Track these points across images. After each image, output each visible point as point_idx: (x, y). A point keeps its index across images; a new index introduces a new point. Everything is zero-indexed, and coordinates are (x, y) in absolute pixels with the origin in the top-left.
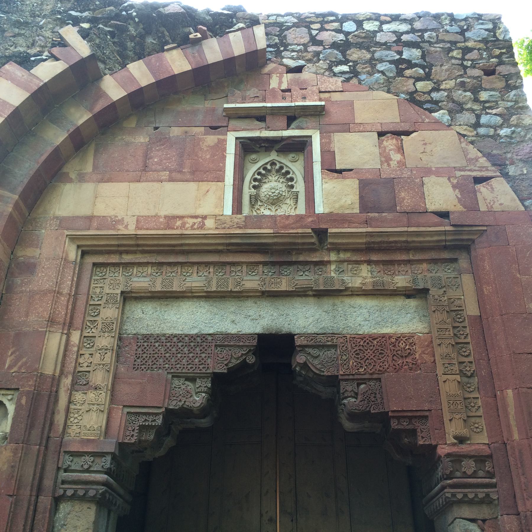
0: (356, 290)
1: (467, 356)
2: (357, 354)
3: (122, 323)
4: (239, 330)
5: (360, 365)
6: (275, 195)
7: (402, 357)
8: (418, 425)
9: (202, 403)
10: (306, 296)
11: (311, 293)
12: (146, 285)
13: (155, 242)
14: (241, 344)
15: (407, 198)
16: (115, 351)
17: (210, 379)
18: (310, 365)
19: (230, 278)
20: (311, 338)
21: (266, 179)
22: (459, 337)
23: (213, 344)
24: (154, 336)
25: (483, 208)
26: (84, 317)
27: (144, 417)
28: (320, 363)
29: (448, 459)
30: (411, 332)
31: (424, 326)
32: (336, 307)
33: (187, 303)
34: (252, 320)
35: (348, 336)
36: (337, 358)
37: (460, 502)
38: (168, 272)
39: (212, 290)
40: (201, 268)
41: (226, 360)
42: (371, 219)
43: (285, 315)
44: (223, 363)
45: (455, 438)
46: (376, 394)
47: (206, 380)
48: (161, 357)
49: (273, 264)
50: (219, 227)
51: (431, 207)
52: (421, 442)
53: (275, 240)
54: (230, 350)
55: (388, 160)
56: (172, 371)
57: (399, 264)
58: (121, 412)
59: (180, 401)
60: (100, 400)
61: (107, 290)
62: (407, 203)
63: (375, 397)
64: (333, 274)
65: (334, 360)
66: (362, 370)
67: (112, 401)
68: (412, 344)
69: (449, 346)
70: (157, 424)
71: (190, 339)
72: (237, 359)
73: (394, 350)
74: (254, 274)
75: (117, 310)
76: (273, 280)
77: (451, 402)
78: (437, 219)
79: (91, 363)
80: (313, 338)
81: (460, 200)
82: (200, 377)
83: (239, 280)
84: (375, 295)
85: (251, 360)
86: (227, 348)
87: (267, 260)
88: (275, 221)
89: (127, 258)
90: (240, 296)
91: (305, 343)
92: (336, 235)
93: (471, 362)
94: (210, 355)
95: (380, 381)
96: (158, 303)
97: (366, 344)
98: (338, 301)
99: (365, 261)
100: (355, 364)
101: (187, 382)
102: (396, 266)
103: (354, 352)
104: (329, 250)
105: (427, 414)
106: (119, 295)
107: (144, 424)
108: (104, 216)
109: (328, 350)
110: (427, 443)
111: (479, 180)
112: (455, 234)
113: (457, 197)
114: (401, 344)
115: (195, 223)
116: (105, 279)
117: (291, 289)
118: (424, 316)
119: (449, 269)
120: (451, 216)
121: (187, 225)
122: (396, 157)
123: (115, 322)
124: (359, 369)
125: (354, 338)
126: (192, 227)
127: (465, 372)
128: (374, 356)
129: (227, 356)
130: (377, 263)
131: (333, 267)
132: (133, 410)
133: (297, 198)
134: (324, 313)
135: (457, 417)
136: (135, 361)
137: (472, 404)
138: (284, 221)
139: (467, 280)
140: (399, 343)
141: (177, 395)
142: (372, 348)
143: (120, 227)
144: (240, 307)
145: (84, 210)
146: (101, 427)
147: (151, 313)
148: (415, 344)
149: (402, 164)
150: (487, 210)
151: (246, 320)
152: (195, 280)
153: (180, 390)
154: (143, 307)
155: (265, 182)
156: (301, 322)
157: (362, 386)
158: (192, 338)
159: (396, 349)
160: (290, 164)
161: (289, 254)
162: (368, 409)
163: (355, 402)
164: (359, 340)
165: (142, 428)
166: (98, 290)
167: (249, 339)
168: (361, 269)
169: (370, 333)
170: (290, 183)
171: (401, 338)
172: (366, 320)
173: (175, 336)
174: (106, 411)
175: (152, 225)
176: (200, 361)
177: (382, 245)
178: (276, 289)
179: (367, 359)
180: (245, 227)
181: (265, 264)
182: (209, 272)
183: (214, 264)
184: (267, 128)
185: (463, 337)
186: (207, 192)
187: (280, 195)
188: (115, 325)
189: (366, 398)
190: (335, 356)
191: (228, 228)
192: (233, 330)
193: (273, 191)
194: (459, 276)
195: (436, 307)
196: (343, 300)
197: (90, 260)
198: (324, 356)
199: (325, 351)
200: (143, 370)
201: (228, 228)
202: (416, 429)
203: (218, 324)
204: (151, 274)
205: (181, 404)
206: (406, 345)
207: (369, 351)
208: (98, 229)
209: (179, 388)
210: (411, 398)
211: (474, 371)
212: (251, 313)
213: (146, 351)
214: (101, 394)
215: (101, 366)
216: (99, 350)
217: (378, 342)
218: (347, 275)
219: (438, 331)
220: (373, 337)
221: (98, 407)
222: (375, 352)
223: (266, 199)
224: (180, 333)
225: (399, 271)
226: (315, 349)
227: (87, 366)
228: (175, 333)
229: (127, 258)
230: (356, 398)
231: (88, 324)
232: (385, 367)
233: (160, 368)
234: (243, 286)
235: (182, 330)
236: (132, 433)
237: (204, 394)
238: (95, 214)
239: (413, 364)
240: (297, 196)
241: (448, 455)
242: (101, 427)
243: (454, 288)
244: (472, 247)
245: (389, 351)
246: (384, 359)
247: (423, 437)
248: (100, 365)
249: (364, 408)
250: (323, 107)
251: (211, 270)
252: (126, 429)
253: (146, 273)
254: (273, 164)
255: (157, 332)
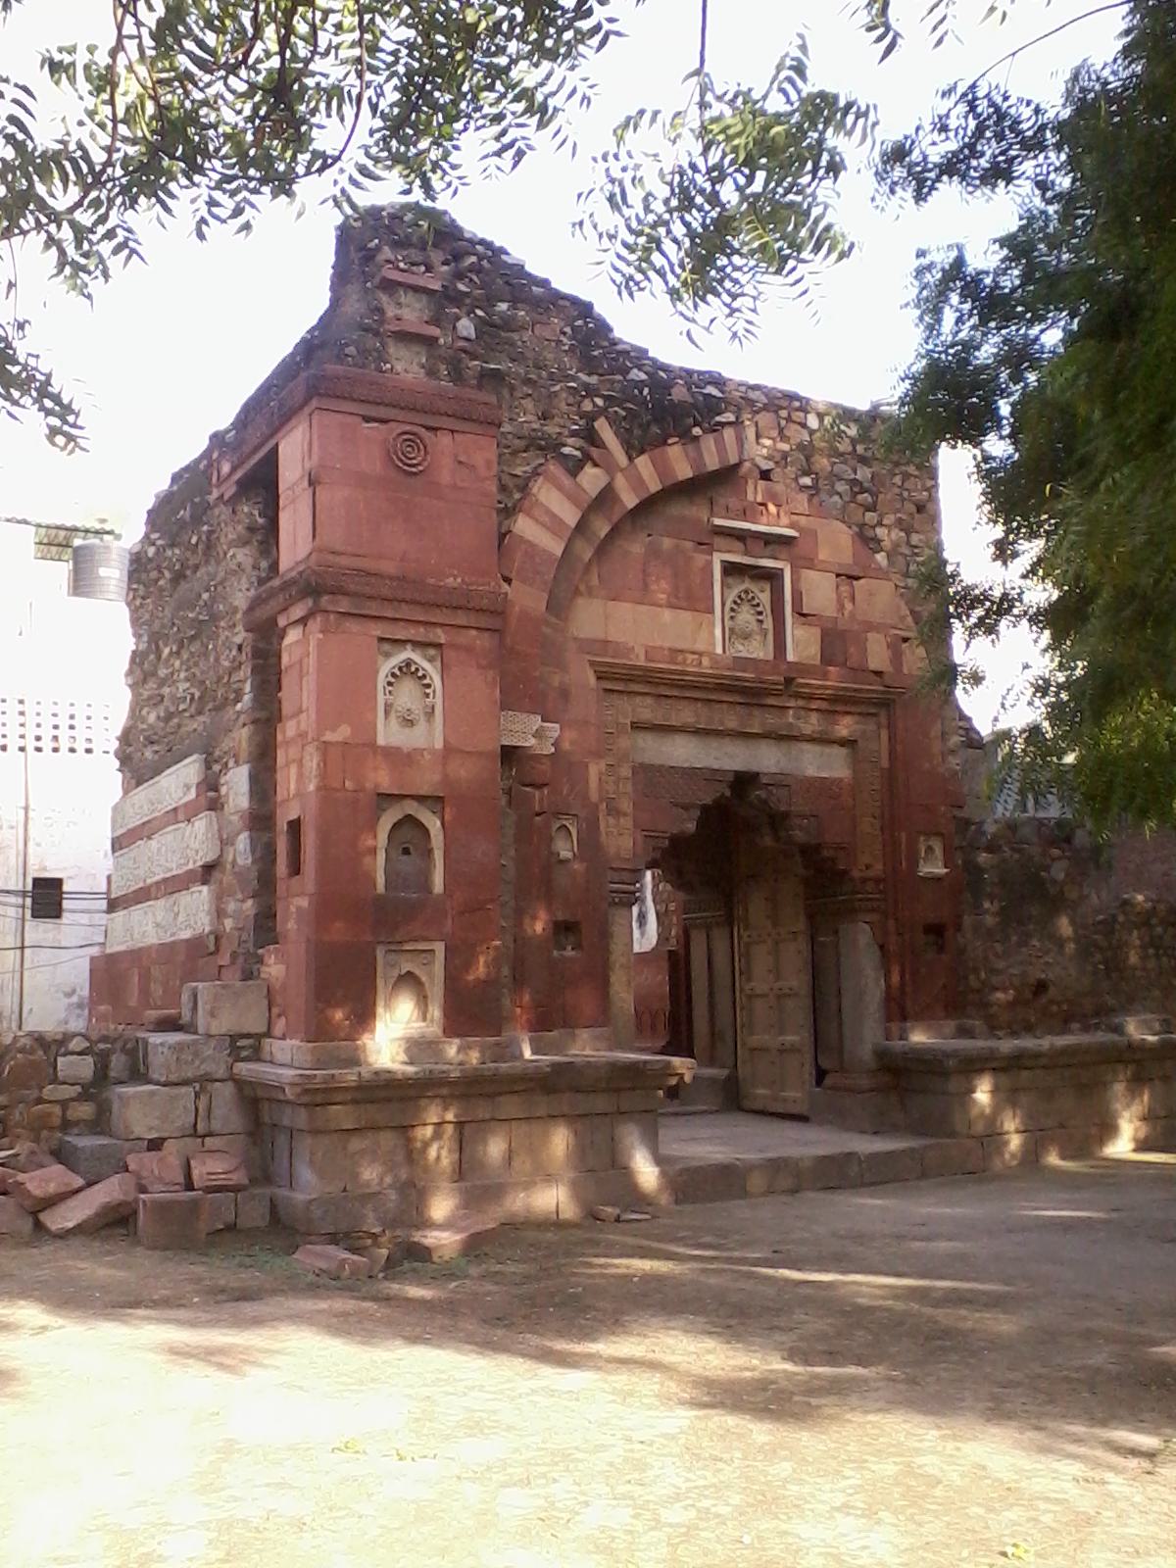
25: (905, 671)
34: (732, 757)
55: (841, 607)
64: (791, 720)
111: (906, 640)
122: (849, 606)
131: (791, 712)
149: (852, 615)
160: (756, 591)
161: (749, 693)
184: (747, 553)
213: (650, 776)
250: (795, 538)
254: (746, 592)
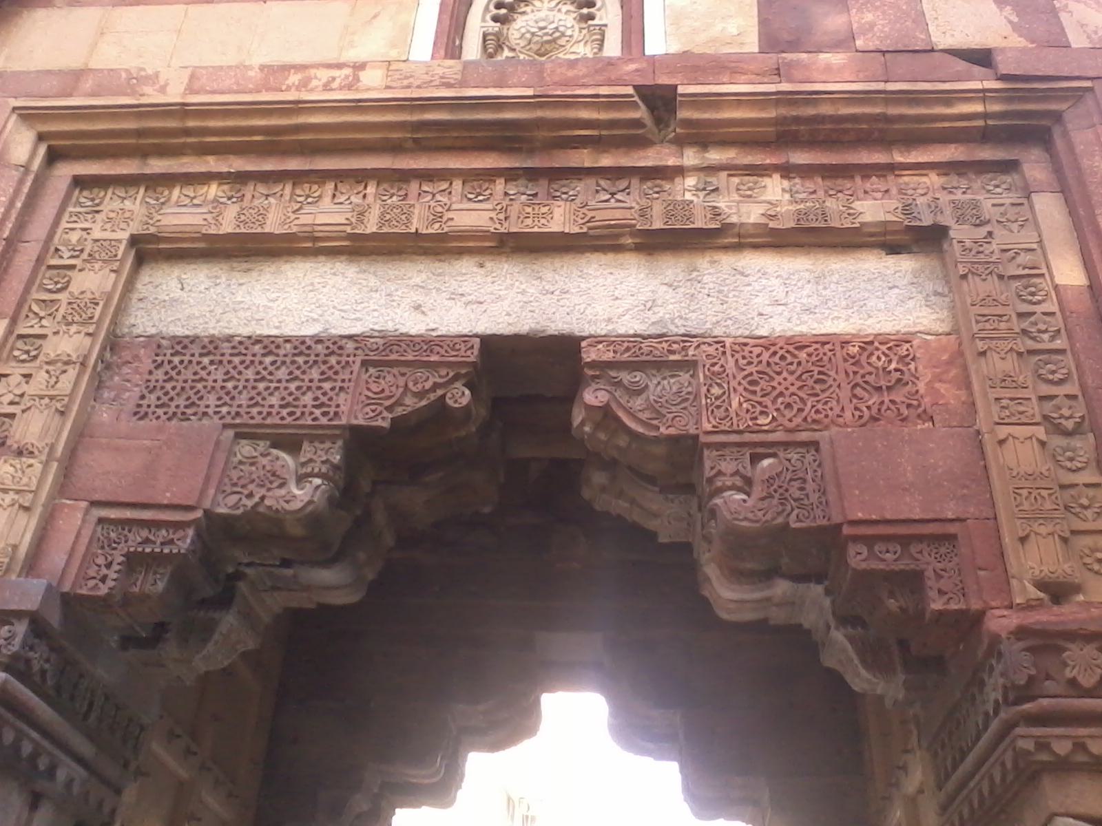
0: (752, 232)
1: (1061, 382)
2: (752, 383)
3: (121, 309)
4: (433, 326)
5: (759, 408)
6: (546, 34)
7: (879, 389)
8: (927, 560)
9: (310, 502)
10: (618, 249)
11: (629, 241)
12: (198, 220)
13: (231, 123)
14: (434, 358)
15: (881, 22)
16: (89, 370)
17: (340, 443)
18: (621, 414)
19: (417, 206)
20: (626, 345)
21: (527, 5)
22: (1034, 339)
23: (358, 360)
24: (202, 341)
25: (1077, 40)
26: (27, 290)
27: (145, 533)
28: (653, 408)
29: (1021, 645)
30: (903, 330)
31: (939, 316)
32: (695, 274)
33: (301, 265)
35: (728, 341)
36: (697, 396)
37: (1063, 767)
38: (257, 194)
39: (368, 231)
40: (343, 187)
41: (390, 397)
42: (790, 65)
43: (557, 293)
44: (380, 404)
45: (1041, 585)
46: (804, 481)
47: (328, 445)
48: (213, 388)
49: (532, 174)
50: (394, 84)
51: (943, 39)
52: (937, 605)
53: (539, 114)
54: (403, 375)
56: (238, 421)
57: (866, 177)
58: (80, 515)
59: (250, 495)
60: (25, 480)
61: (97, 234)
62: (882, 31)
63: (802, 489)
65: (687, 400)
66: (763, 420)
67: (64, 486)
68: (908, 360)
69: (1009, 355)
70: (175, 551)
71: (295, 348)
72: (421, 395)
73: (855, 373)
74: (481, 198)
75: (113, 275)
76: (529, 210)
77: (1024, 492)
78: (961, 65)
79: (22, 395)
80: (631, 345)
81: (1016, 28)
82: (312, 439)
83: (439, 209)
84: (802, 246)
85: (460, 397)
86: (395, 371)
87: (517, 165)
88: (541, 72)
89: (157, 166)
90: (439, 247)
91: (608, 356)
92: (697, 101)
93: (1074, 397)
94: (345, 385)
95: (817, 450)
96: (225, 266)
97: (776, 359)
98: (703, 262)
99: (776, 168)
100: (745, 405)
101: (275, 451)
102: (858, 179)
103: (744, 378)
104: (681, 142)
105: (952, 529)
106: (125, 242)
107: (140, 549)
108: (112, 70)
109: (672, 376)
110: (953, 606)
112: (1009, 100)
113: (1010, 22)
114: (874, 358)
115: (334, 79)
116: (97, 212)
117: (576, 230)
118: (936, 294)
119: (997, 186)
120: (999, 58)
121: (314, 83)
123: (101, 303)
124: (756, 418)
125: (746, 345)
126: (327, 87)
127: (1057, 421)
128: (800, 388)
129: (393, 389)
130: (806, 172)
131: (691, 181)
132: (113, 514)
133: (602, 41)
134: (665, 288)
135: (1043, 530)
136: (143, 397)
137: (1085, 501)
138: (563, 70)
139: (1049, 207)
140: (868, 357)
141: (243, 482)
142: (793, 368)
143: (148, 90)
144: (439, 275)
145: (71, 60)
146: (15, 547)
147: (202, 288)
148: (913, 359)
150: (1090, 46)
151: (451, 303)
152: (328, 211)
153: (253, 468)
154: (184, 276)
155: (524, 13)
156: (599, 309)
157: (766, 462)
158: (301, 345)
159: (862, 372)
162: (780, 520)
163: (744, 501)
164: (757, 350)
165: (134, 562)
166: (74, 237)
167: (457, 347)
168: (764, 187)
169: (789, 334)
170: (585, 11)
171: (876, 344)
172: (777, 303)
173: (258, 341)
174: (38, 510)
175: (228, 83)
176: (316, 399)
177: (821, 127)
178: (536, 229)
179: (781, 394)
180: (463, 84)
181: (510, 175)
182: (365, 196)
183: (380, 176)
185: (1046, 336)
186: (375, 17)
187: (557, 34)
188: (99, 309)
189: (775, 491)
190: (690, 389)
191: (419, 87)
192: (414, 325)
193: (542, 24)
194: (1025, 201)
195: (969, 265)
196: (716, 258)
197: (66, 171)
198: (659, 388)
199: (664, 378)
200: (158, 418)
201: (419, 87)
202: (922, 572)
203: (376, 314)
204: (215, 200)
205: (249, 503)
206: (890, 361)
207: (785, 374)
208: (93, 94)
209: (252, 464)
210: (905, 490)
211: (1083, 417)
212: (467, 287)
214: (30, 466)
215: (47, 400)
216: (47, 363)
217: (810, 355)
218: (726, 199)
219: (977, 322)
220: (798, 344)
221: (16, 497)
222: (804, 377)
223: (523, 43)
224: (274, 332)
225: (866, 192)
226: (635, 373)
227: (11, 403)
228: (258, 332)
229: (157, 166)
230: (748, 494)
231: (35, 308)
232: (830, 413)
233: (205, 414)
234: (450, 223)
235: (277, 328)
236: (104, 571)
237: (318, 481)
238: (92, 65)
239: (909, 406)
240: (603, 35)
241: (1021, 632)
242: (15, 547)
243: (1015, 227)
244: (1057, 132)
245: (842, 375)
246: (827, 394)
247: (941, 592)
248: (41, 397)
249: (769, 517)
251: (371, 189)
252: (88, 557)
253: (202, 198)
255: (212, 332)
